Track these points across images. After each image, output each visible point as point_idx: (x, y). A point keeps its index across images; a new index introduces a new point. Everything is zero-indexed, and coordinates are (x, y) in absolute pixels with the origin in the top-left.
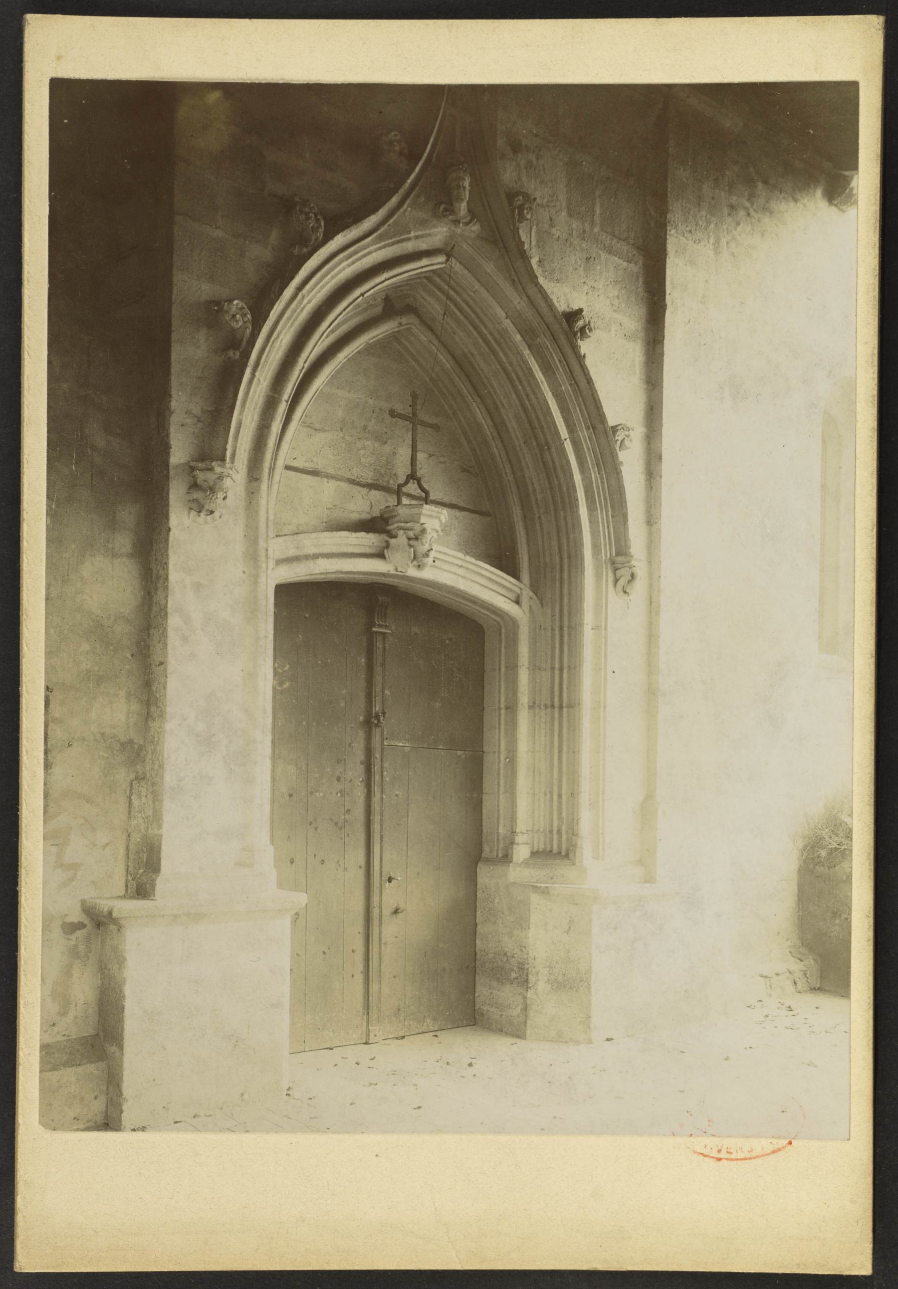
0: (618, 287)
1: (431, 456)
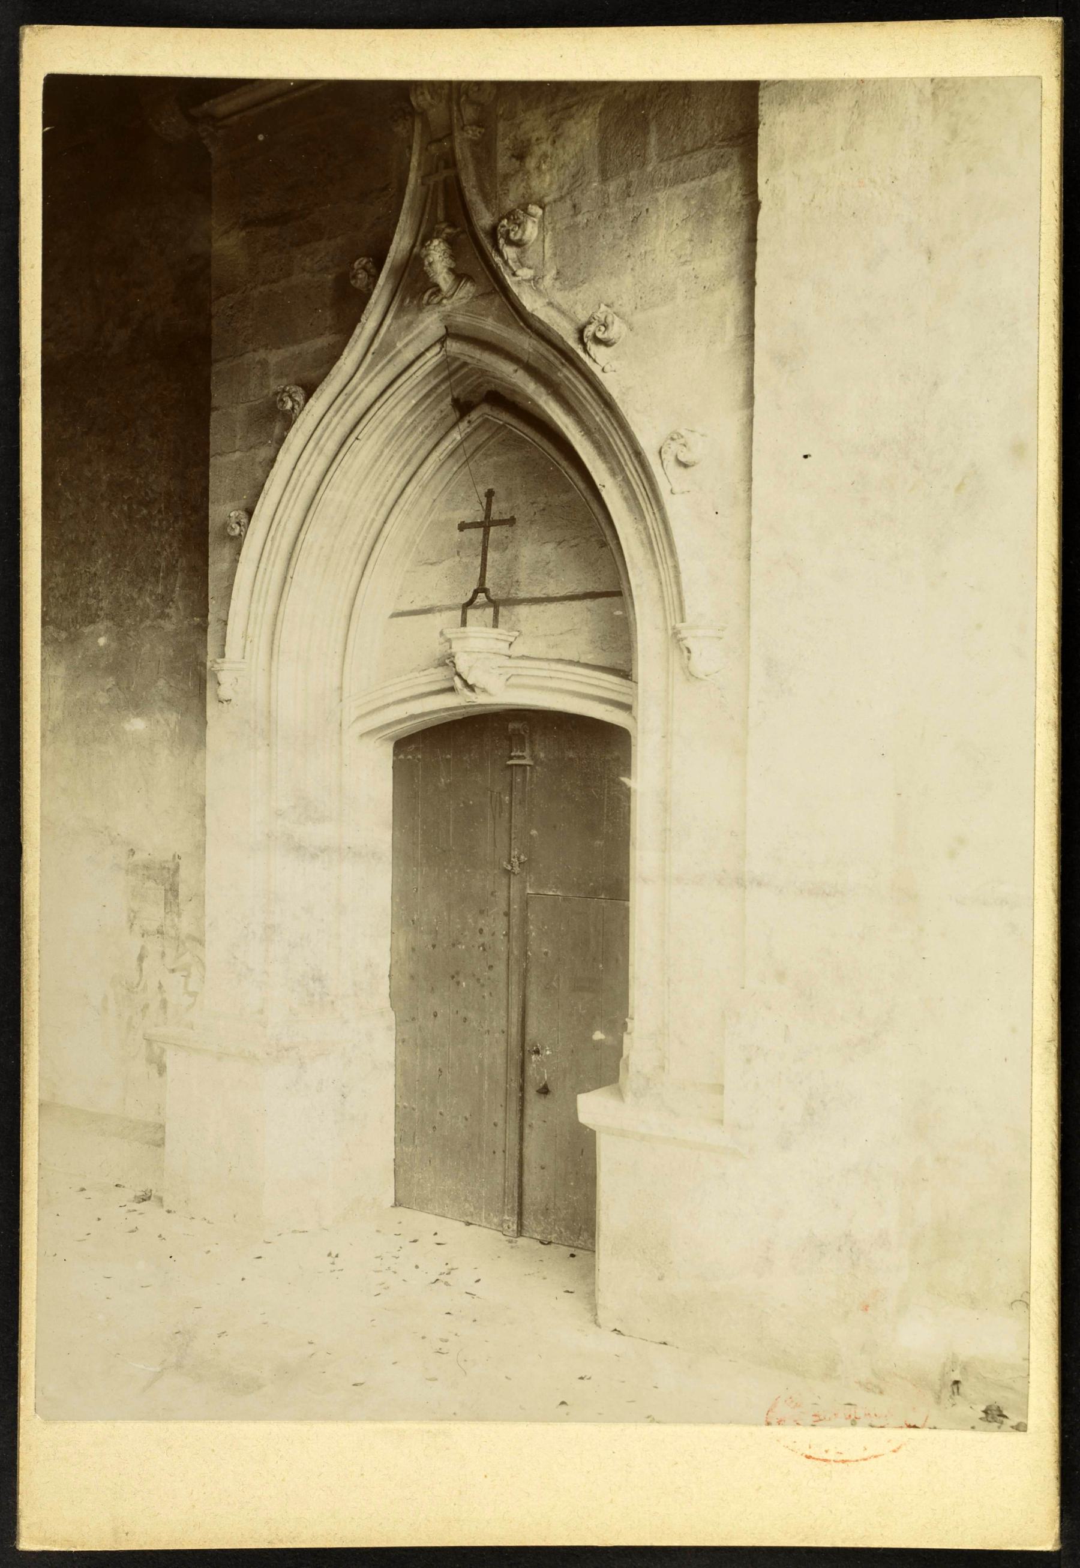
0: (690, 225)
1: (560, 543)
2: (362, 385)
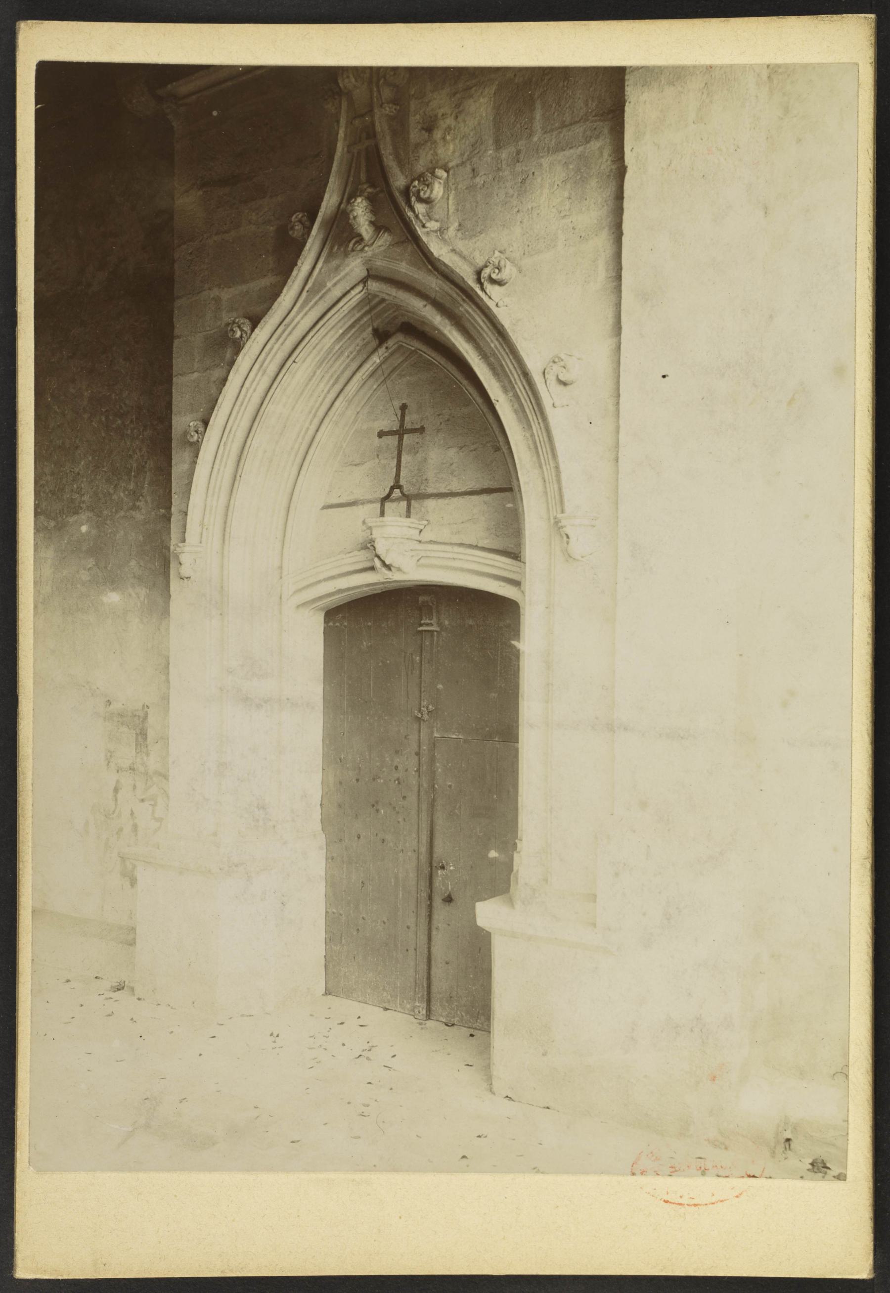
0: (568, 186)
1: (461, 448)
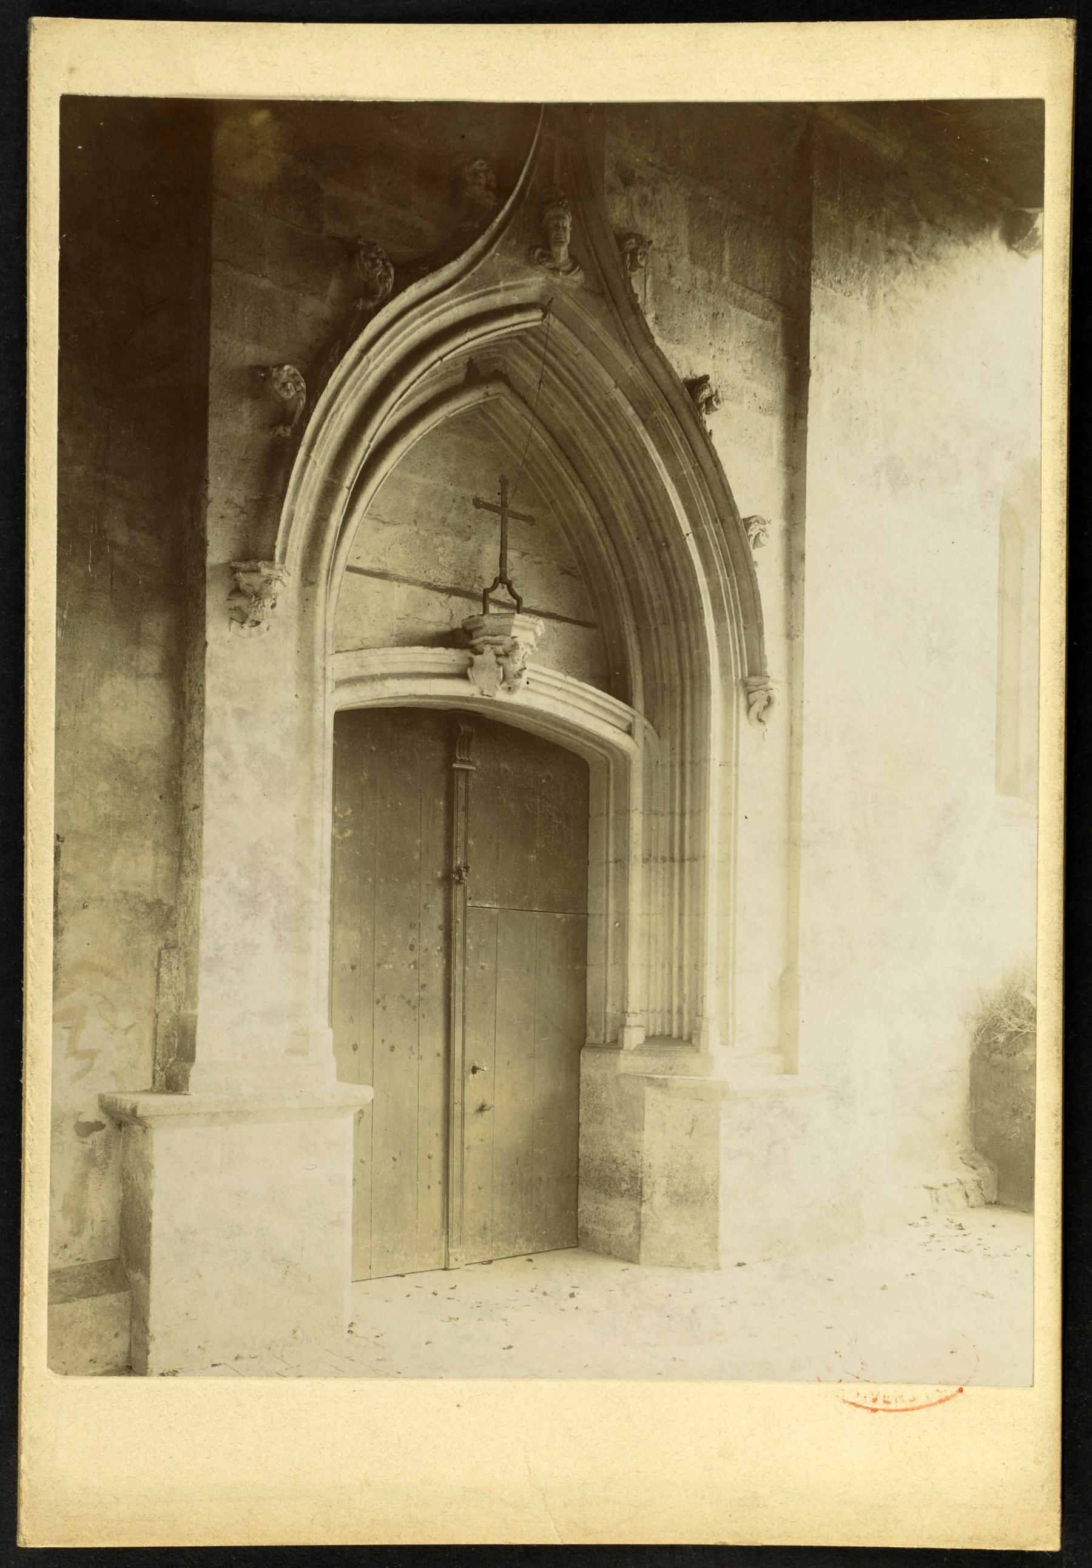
0: (751, 349)
1: (524, 554)
2: (452, 302)
